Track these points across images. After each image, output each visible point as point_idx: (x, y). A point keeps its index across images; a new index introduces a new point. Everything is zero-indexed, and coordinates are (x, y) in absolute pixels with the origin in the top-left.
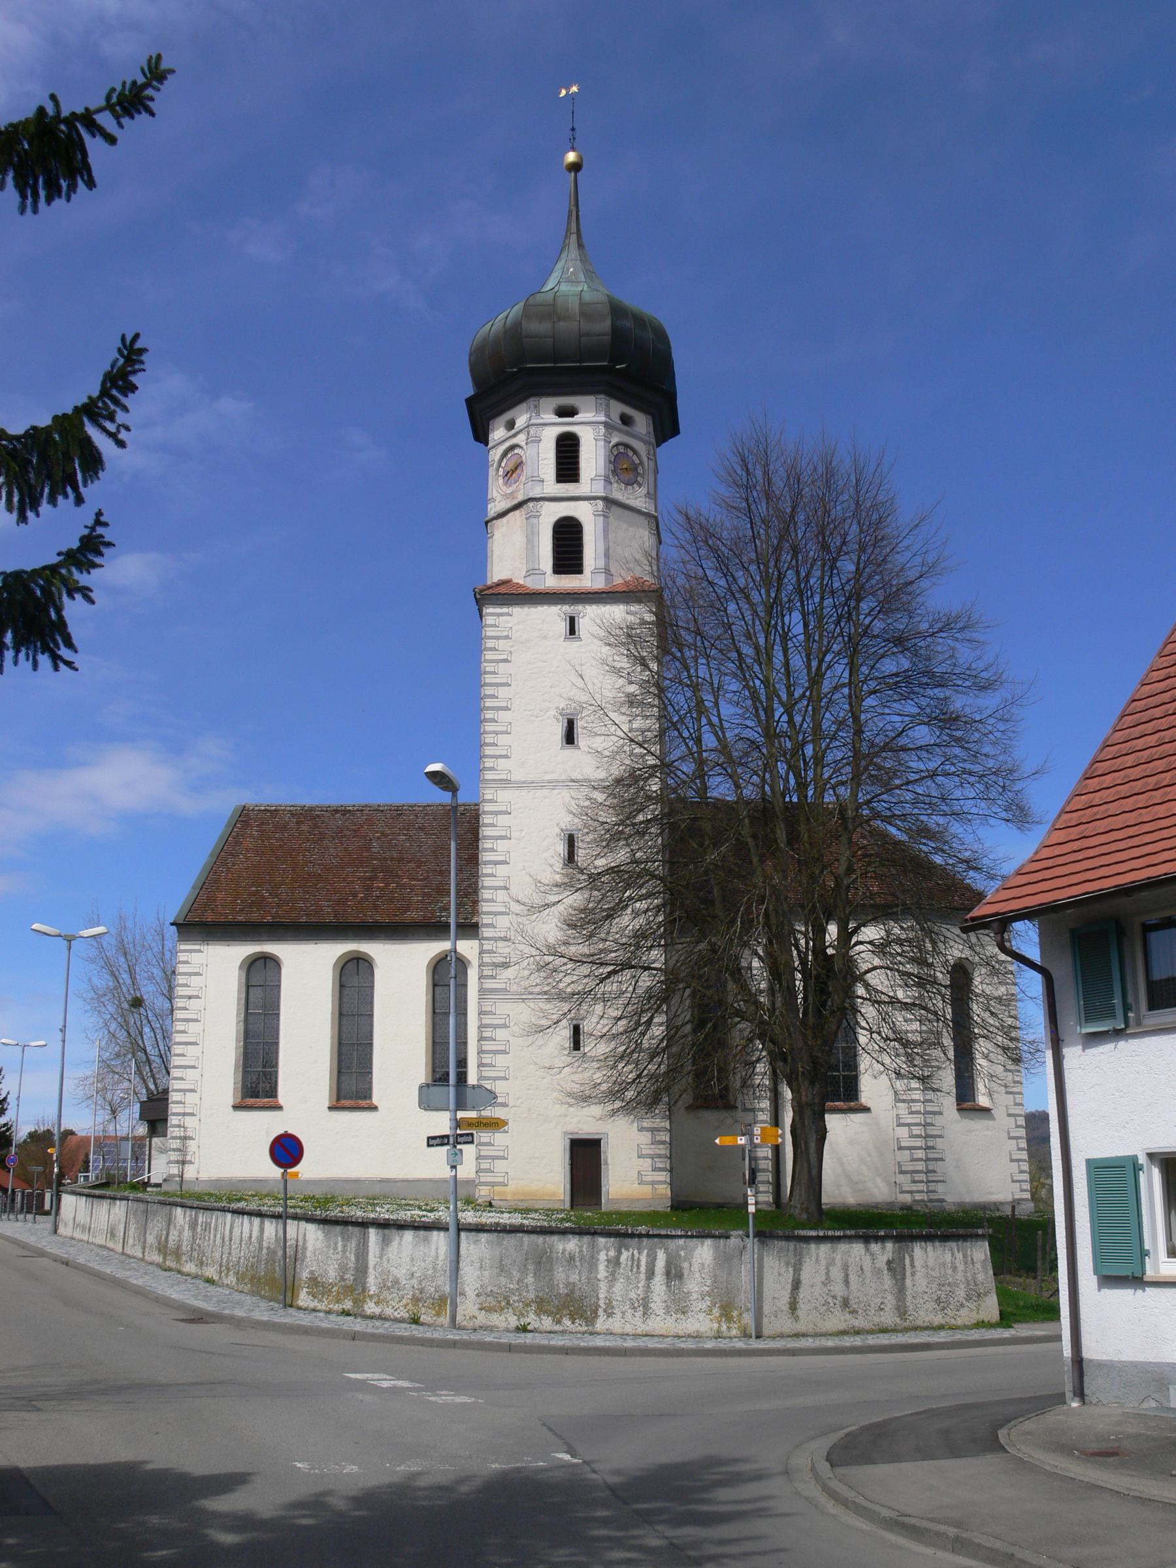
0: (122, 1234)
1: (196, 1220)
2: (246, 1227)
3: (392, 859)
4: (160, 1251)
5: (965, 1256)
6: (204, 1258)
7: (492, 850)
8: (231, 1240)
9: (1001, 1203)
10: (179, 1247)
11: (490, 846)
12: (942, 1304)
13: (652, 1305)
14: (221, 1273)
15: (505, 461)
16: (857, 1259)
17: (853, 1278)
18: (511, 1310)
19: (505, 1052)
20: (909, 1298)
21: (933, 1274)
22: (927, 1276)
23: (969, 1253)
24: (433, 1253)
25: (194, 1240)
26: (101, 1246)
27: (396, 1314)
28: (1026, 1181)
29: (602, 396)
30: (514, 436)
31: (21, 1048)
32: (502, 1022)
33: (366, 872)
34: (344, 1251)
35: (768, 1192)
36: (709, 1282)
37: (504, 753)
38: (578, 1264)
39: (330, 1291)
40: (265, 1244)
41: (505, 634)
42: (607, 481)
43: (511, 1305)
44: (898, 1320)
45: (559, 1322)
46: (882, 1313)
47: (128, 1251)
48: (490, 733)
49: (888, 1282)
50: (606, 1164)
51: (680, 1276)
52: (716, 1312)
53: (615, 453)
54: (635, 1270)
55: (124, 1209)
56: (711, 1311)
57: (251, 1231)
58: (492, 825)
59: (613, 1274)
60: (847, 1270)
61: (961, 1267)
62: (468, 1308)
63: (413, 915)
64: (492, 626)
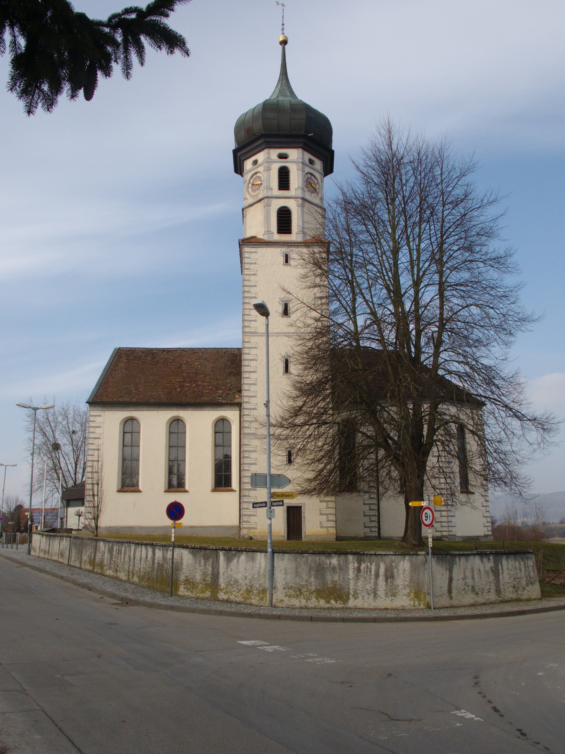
0: (67, 555)
1: (112, 548)
2: (143, 552)
3: (193, 373)
4: (90, 564)
5: (525, 564)
6: (118, 568)
7: (248, 366)
8: (134, 558)
9: (479, 536)
10: (102, 562)
11: (247, 364)
12: (516, 589)
13: (378, 592)
14: (129, 576)
15: (252, 180)
16: (478, 566)
17: (476, 576)
18: (302, 596)
19: (255, 464)
20: (501, 585)
21: (511, 572)
22: (509, 574)
23: (526, 562)
24: (258, 566)
25: (111, 559)
26: (55, 561)
27: (236, 599)
28: (490, 526)
29: (301, 149)
30: (258, 167)
31: (5, 467)
32: (254, 449)
33: (181, 379)
34: (205, 565)
35: (376, 531)
36: (408, 579)
37: (254, 319)
38: (338, 571)
39: (197, 587)
40: (156, 561)
41: (254, 262)
42: (303, 190)
43: (302, 593)
44: (497, 597)
45: (328, 602)
46: (490, 594)
47: (72, 563)
48: (247, 309)
49: (492, 578)
50: (304, 517)
51: (392, 577)
52: (412, 595)
53: (307, 177)
54: (369, 573)
55: (68, 543)
56: (409, 595)
57: (147, 554)
58: (248, 354)
59: (357, 576)
60: (473, 571)
61: (523, 569)
62: (279, 595)
63: (205, 399)
64: (247, 258)
